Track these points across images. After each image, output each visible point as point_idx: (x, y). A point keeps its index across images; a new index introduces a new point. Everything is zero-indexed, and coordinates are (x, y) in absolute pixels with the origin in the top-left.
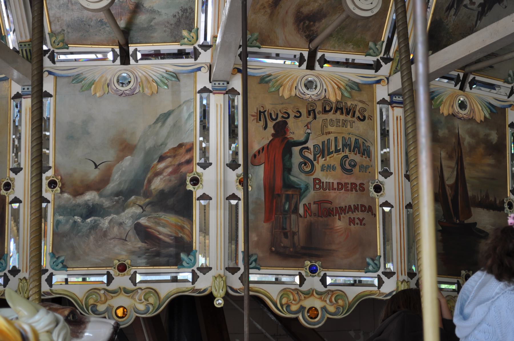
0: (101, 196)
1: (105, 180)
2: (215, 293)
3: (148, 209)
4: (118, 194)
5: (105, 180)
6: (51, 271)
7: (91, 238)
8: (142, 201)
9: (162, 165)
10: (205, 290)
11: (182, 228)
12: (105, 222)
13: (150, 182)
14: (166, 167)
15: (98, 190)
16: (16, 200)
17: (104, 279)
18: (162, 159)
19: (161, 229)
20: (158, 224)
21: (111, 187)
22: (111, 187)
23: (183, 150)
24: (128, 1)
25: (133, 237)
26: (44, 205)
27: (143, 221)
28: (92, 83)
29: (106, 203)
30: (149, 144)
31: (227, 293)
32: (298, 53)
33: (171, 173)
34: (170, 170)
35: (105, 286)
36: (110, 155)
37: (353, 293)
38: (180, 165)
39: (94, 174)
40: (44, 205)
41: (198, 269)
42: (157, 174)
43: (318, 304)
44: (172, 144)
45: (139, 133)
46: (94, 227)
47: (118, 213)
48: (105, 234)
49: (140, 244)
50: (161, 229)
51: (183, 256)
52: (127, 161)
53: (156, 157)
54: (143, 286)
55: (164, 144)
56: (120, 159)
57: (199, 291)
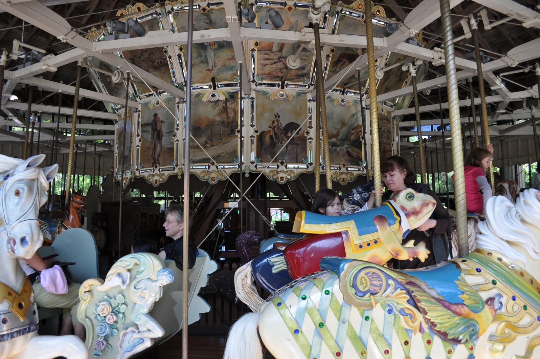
0: (337, 140)
1: (338, 134)
2: (246, 172)
3: (350, 146)
4: (342, 140)
5: (338, 134)
6: (323, 165)
7: (335, 154)
8: (348, 143)
9: (353, 131)
10: (311, 172)
11: (359, 153)
12: (338, 149)
13: (350, 137)
14: (355, 132)
15: (336, 138)
16: (311, 138)
17: (276, 167)
18: (353, 129)
19: (353, 153)
20: (353, 151)
21: (340, 137)
22: (340, 137)
23: (359, 127)
24: (533, 92)
25: (346, 155)
26: (242, 139)
27: (349, 150)
28: (334, 100)
29: (339, 143)
30: (350, 124)
31: (250, 172)
32: (209, 84)
33: (356, 135)
34: (355, 133)
35: (276, 169)
36: (339, 126)
37: (355, 173)
38: (358, 132)
39: (335, 132)
40: (242, 139)
41: (309, 164)
42: (353, 134)
43: (284, 175)
44: (356, 125)
45: (347, 119)
46: (335, 150)
47: (342, 146)
48: (338, 153)
49: (348, 158)
50: (353, 153)
51: (360, 162)
52: (344, 129)
53: (352, 128)
54: (350, 171)
55: (354, 124)
56: (342, 128)
57: (309, 172)
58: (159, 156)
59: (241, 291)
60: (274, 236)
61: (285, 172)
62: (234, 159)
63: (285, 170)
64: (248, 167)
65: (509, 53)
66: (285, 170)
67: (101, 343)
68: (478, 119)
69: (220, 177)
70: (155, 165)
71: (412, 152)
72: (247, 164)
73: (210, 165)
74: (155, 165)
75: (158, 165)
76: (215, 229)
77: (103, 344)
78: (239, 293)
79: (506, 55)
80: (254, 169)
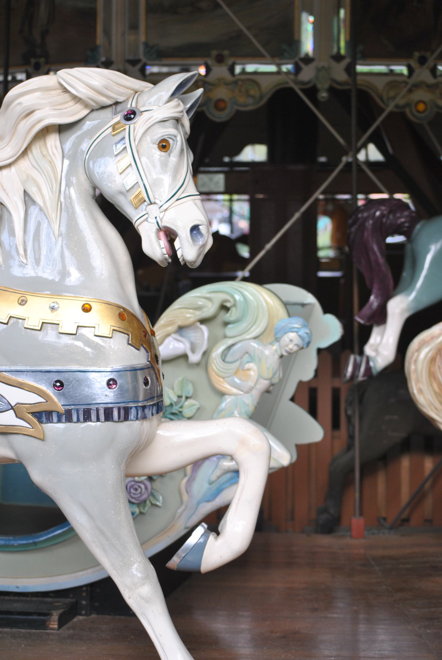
2: (319, 86)
58: (45, 34)
59: (425, 387)
60: (233, 417)
61: (431, 87)
62: (285, 47)
63: (430, 80)
64: (327, 70)
65: (59, 72)
66: (430, 80)
67: (143, 486)
68: (149, 569)
69: (242, 100)
70: (33, 61)
71: (112, 512)
72: (324, 64)
73: (210, 62)
74: (33, 61)
75: (42, 60)
76: (261, 248)
77: (146, 488)
78: (420, 391)
79: (56, 74)
80: (342, 76)
